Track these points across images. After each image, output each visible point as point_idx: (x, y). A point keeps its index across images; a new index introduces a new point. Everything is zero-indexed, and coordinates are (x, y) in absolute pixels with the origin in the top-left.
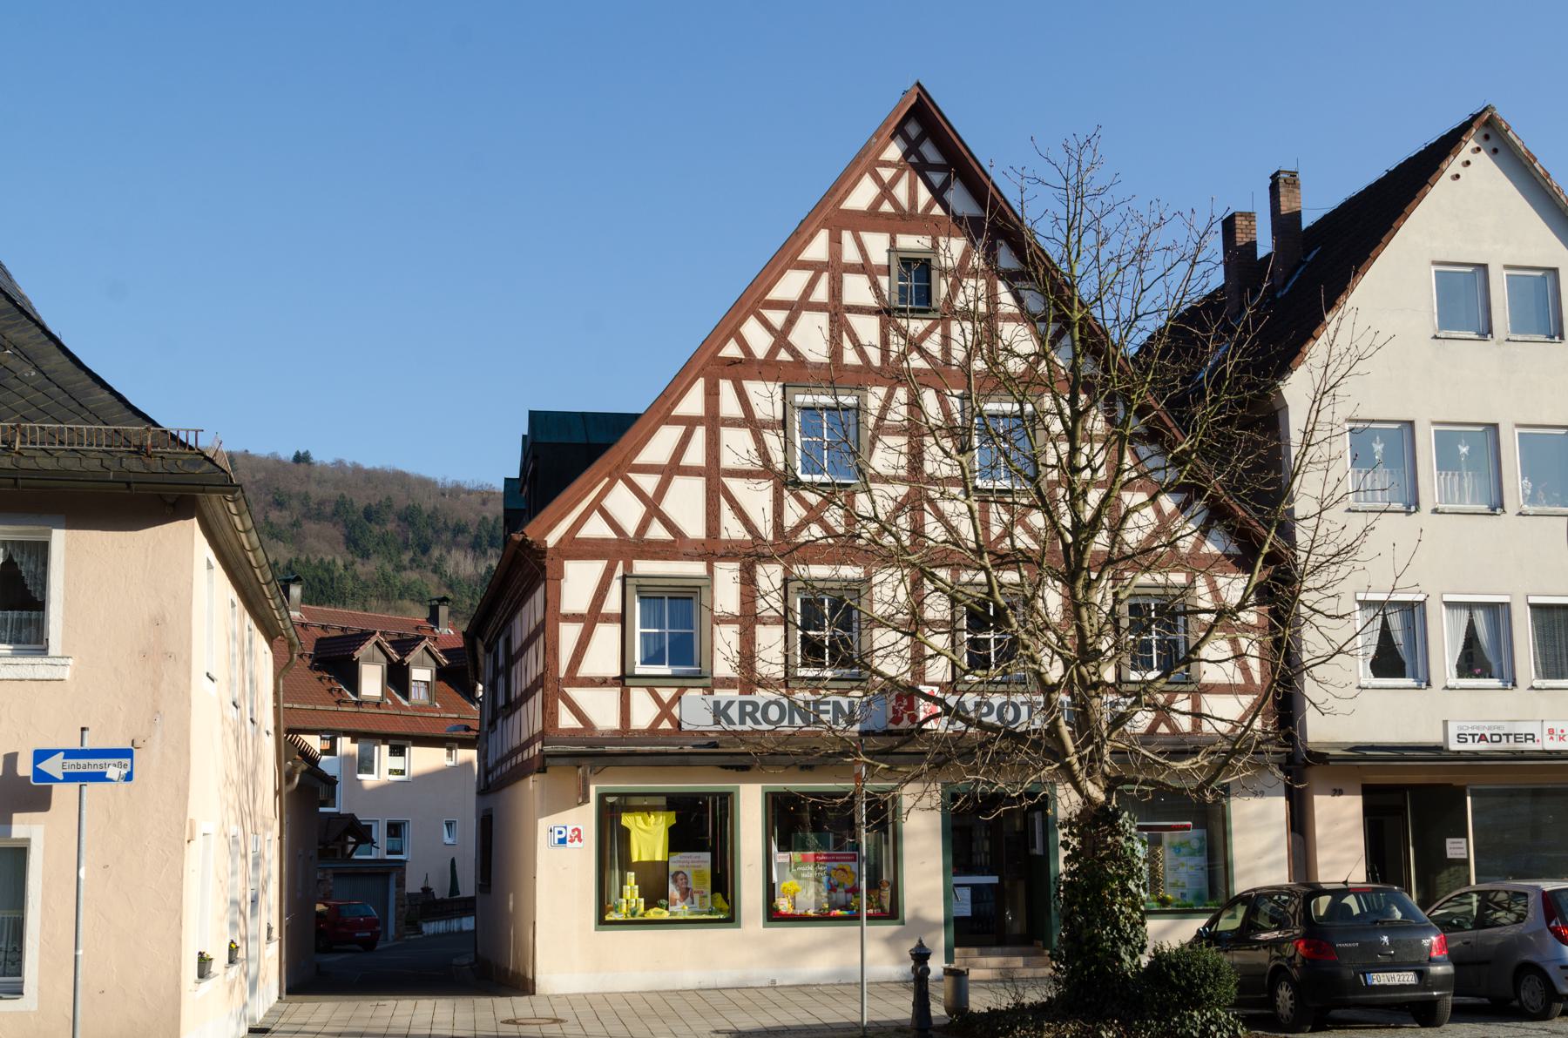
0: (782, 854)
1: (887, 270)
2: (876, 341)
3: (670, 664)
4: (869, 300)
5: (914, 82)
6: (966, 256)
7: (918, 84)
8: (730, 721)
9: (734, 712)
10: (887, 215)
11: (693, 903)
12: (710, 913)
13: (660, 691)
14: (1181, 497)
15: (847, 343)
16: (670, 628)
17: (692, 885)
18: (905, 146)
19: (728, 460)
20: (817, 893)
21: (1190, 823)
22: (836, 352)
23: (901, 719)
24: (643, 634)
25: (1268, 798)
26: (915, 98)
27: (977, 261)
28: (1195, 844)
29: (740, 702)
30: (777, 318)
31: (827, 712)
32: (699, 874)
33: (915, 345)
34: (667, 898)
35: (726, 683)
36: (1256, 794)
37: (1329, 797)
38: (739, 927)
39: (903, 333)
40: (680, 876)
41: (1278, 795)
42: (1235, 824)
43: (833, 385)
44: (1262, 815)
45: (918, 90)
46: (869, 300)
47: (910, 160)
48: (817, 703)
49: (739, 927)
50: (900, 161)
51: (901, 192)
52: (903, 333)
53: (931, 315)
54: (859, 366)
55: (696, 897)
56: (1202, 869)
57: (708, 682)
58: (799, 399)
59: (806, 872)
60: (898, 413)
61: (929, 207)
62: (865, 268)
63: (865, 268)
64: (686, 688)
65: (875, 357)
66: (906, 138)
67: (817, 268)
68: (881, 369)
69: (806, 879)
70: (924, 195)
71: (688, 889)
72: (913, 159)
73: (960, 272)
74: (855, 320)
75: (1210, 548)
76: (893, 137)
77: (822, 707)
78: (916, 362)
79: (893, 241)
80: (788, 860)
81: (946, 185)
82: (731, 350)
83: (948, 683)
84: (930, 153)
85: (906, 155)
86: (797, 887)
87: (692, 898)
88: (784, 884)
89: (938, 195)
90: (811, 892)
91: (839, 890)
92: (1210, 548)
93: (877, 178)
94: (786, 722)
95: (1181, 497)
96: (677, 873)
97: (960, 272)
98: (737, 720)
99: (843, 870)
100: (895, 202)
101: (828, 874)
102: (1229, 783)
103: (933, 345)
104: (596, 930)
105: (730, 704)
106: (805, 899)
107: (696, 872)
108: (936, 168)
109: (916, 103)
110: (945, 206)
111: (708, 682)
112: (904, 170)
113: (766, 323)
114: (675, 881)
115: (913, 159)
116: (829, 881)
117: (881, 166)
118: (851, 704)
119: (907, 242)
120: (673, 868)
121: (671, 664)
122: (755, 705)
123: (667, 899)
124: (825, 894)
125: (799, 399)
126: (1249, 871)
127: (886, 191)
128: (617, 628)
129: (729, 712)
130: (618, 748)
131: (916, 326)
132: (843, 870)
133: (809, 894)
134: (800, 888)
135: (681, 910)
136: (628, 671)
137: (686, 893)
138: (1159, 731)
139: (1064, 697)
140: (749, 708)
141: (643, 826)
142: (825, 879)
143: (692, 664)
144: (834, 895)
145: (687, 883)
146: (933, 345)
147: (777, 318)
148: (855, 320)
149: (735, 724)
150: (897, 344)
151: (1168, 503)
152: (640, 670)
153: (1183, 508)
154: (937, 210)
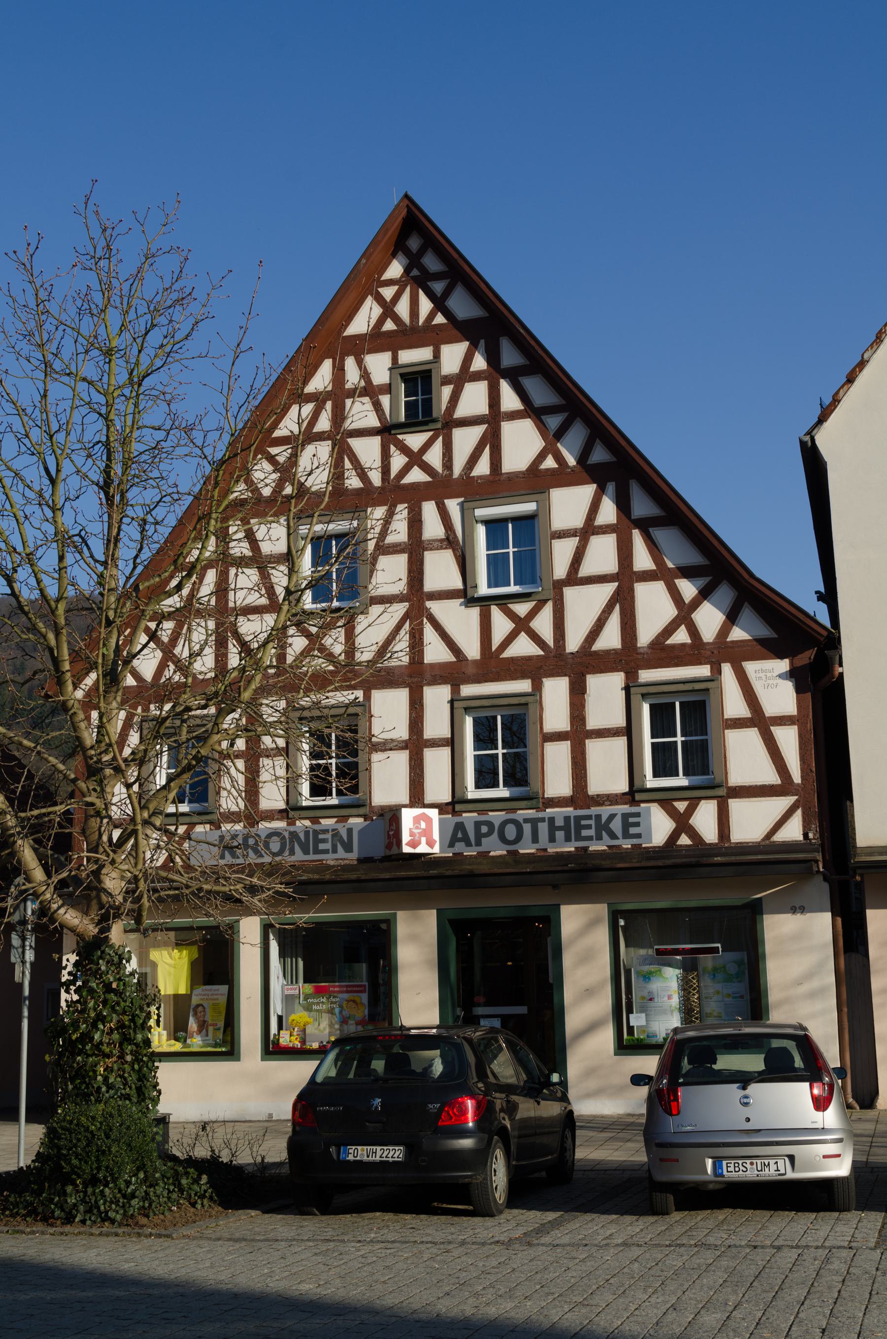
0: (306, 985)
1: (388, 389)
2: (378, 463)
3: (686, 774)
4: (373, 421)
5: (402, 194)
6: (468, 360)
7: (406, 196)
8: (613, 836)
9: (616, 825)
10: (390, 333)
11: (207, 1035)
12: (215, 1046)
13: (677, 804)
14: (702, 582)
15: (347, 464)
16: (676, 742)
17: (209, 1018)
18: (406, 261)
19: (431, 584)
20: (331, 1025)
21: (719, 945)
22: (338, 476)
23: (419, 843)
24: (477, 757)
25: (809, 915)
26: (406, 210)
27: (479, 363)
28: (732, 969)
29: (623, 815)
30: (282, 453)
31: (589, 827)
32: (215, 1006)
33: (416, 459)
34: (186, 1031)
35: (232, 817)
36: (794, 910)
37: (789, 916)
38: (238, 1059)
39: (404, 449)
40: (200, 1009)
41: (822, 910)
42: (770, 945)
43: (329, 515)
44: (798, 937)
45: (406, 202)
46: (373, 421)
47: (411, 275)
48: (578, 819)
49: (238, 1059)
50: (402, 276)
51: (403, 308)
52: (404, 449)
53: (432, 426)
54: (361, 489)
55: (211, 1029)
56: (742, 997)
57: (722, 792)
58: (480, 512)
59: (318, 1004)
60: (399, 532)
61: (431, 316)
62: (369, 390)
63: (369, 390)
64: (195, 824)
65: (376, 478)
66: (407, 253)
67: (318, 399)
68: (382, 488)
69: (317, 1011)
70: (425, 305)
71: (204, 1022)
72: (415, 272)
73: (465, 376)
74: (356, 444)
75: (738, 634)
76: (394, 255)
77: (583, 822)
78: (416, 476)
79: (395, 359)
80: (297, 991)
81: (447, 292)
82: (240, 490)
83: (447, 804)
84: (432, 263)
85: (407, 271)
86: (308, 1020)
87: (207, 1031)
88: (292, 1017)
89: (439, 304)
90: (325, 1023)
91: (351, 1022)
92: (738, 634)
93: (379, 299)
94: (287, 853)
95: (702, 582)
96: (198, 1006)
97: (465, 376)
98: (619, 833)
99: (354, 1001)
100: (397, 319)
101: (341, 1006)
102: (760, 899)
103: (434, 457)
104: (262, 1060)
105: (612, 817)
106: (316, 1032)
107: (214, 1004)
108: (437, 277)
109: (407, 216)
110: (447, 314)
111: (722, 792)
112: (406, 286)
113: (272, 459)
114: (195, 1014)
115: (415, 272)
116: (341, 1012)
117: (383, 286)
118: (350, 831)
119: (408, 356)
120: (195, 1001)
121: (190, 802)
122: (490, 824)
123: (186, 1032)
124: (337, 1026)
125: (480, 512)
126: (787, 1001)
127: (388, 310)
128: (446, 752)
129: (611, 826)
130: (760, 857)
131: (415, 441)
132: (354, 1001)
133: (322, 1026)
134: (310, 1020)
135: (196, 1043)
136: (458, 794)
137: (203, 1026)
138: (679, 842)
139: (199, 829)
140: (484, 829)
141: (169, 961)
142: (337, 1011)
143: (708, 774)
144: (345, 1027)
145: (204, 1016)
146: (434, 457)
147: (282, 453)
148: (356, 444)
149: (618, 838)
150: (398, 461)
151: (688, 589)
152: (651, 782)
153: (704, 594)
154: (440, 319)
